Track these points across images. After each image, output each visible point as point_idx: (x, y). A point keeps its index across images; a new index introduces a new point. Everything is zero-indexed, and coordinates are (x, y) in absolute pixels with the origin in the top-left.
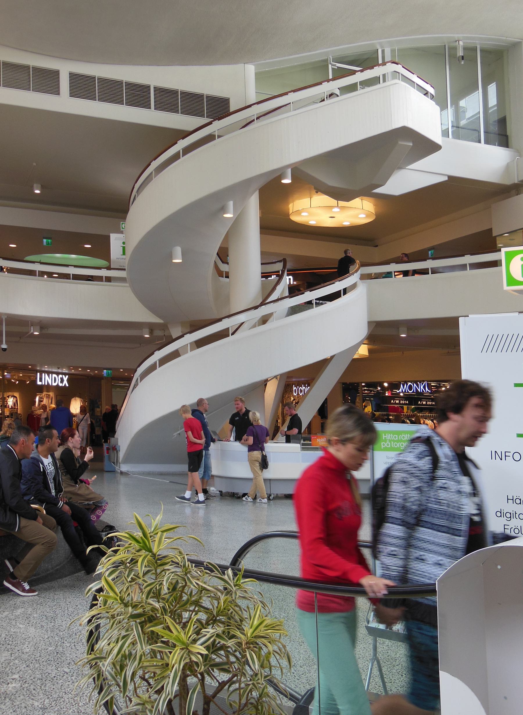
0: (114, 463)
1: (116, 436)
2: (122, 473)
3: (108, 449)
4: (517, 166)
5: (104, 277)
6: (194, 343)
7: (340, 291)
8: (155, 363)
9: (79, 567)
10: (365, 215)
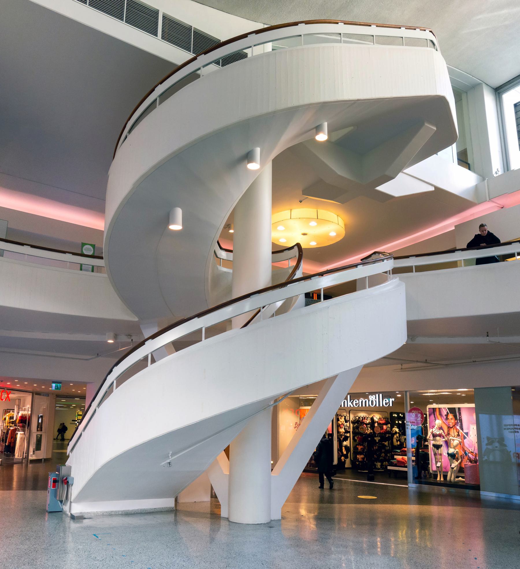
0: (61, 502)
2: (73, 517)
3: (55, 481)
6: (172, 344)
8: (200, 331)
9: (81, 520)
10: (316, 243)
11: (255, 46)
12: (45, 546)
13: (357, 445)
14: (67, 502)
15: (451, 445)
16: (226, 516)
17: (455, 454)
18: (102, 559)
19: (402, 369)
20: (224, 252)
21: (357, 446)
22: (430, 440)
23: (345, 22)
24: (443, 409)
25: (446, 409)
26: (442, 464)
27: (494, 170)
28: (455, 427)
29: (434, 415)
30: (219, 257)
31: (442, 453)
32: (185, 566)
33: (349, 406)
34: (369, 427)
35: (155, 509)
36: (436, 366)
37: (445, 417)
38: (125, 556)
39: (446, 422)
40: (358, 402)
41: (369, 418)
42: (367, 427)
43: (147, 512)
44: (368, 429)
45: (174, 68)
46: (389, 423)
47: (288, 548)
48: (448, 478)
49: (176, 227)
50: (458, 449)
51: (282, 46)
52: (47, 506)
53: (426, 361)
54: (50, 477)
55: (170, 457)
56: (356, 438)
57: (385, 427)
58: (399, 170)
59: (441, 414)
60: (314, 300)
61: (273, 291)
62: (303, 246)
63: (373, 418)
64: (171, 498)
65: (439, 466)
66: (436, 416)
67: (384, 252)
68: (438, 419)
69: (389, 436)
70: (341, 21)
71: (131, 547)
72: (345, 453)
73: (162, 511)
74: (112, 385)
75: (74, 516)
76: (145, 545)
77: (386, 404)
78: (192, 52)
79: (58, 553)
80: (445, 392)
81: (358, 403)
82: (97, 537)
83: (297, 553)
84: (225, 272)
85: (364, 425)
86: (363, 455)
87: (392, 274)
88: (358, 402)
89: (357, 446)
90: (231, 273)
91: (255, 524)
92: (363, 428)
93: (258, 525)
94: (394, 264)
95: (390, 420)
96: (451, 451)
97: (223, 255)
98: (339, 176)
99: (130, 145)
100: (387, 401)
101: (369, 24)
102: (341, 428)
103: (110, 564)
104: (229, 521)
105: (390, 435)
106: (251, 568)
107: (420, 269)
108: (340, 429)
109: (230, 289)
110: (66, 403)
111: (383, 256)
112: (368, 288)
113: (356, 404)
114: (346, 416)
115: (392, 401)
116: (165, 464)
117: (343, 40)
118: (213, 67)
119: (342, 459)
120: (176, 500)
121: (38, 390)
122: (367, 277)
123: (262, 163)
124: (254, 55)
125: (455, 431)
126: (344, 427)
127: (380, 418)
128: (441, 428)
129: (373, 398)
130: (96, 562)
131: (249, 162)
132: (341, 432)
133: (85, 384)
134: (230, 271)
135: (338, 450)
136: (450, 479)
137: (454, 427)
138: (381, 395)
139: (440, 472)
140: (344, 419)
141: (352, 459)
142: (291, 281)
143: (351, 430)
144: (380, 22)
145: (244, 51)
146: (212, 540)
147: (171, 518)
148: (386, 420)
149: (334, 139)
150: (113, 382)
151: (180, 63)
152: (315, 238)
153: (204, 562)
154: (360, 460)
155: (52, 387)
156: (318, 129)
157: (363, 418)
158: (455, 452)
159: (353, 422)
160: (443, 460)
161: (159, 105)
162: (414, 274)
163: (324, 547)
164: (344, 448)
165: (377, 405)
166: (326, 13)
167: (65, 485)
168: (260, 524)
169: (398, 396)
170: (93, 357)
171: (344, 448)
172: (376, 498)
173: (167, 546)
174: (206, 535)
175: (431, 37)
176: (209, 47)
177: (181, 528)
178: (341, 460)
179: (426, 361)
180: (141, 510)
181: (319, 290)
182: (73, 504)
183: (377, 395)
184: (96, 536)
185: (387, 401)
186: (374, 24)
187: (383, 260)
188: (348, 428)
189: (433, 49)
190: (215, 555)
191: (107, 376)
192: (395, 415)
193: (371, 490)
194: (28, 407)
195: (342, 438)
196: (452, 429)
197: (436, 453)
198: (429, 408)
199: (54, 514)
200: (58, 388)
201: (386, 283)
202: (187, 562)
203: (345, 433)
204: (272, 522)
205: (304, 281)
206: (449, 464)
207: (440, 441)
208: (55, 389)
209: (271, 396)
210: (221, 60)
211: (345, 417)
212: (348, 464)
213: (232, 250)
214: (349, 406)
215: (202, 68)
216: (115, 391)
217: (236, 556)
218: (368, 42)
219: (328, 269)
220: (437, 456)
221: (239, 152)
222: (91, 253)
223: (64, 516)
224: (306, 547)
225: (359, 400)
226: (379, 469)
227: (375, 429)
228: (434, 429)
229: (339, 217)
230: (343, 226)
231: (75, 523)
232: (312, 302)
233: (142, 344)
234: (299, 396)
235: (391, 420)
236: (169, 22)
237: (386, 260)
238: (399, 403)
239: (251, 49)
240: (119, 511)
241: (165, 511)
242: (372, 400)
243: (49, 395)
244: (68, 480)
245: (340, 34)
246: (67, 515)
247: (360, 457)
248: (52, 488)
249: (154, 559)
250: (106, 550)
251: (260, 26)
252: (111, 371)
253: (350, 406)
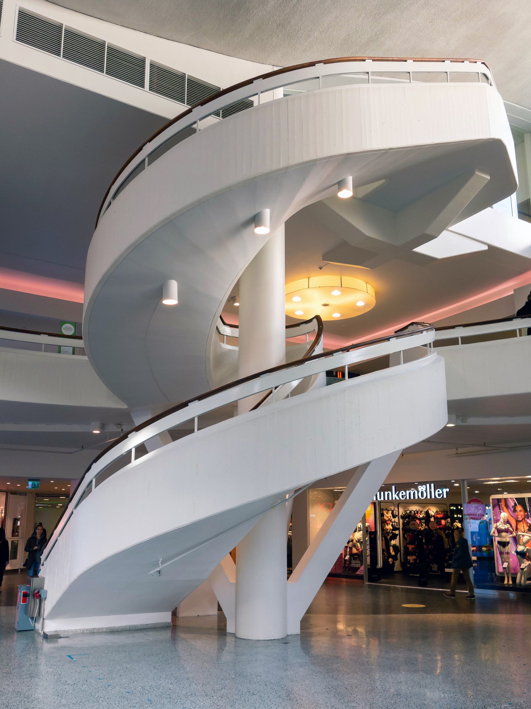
1: (40, 574)
2: (46, 637)
3: (25, 595)
9: (56, 640)
11: (262, 92)
12: (8, 669)
13: (407, 544)
14: (40, 620)
15: (521, 541)
16: (233, 632)
17: (526, 553)
18: (74, 683)
19: (457, 453)
20: (228, 328)
21: (408, 546)
22: (495, 537)
23: (374, 58)
24: (510, 500)
25: (514, 500)
26: (511, 565)
28: (525, 520)
29: (499, 507)
30: (222, 333)
31: (510, 551)
32: (171, 689)
33: (394, 499)
34: (423, 522)
35: (147, 625)
36: (497, 449)
37: (512, 509)
38: (101, 679)
39: (514, 515)
40: (404, 494)
41: (423, 512)
42: (420, 522)
43: (137, 629)
44: (422, 525)
45: (167, 123)
46: (448, 517)
47: (301, 667)
48: (518, 581)
49: (171, 301)
50: (529, 547)
51: (295, 90)
52: (16, 623)
53: (485, 444)
54: (19, 591)
55: (160, 565)
56: (406, 536)
57: (443, 522)
58: (443, 227)
59: (507, 506)
60: (338, 379)
61: (288, 370)
62: (323, 319)
63: (428, 512)
64: (167, 612)
65: (506, 567)
66: (501, 508)
67: (424, 323)
68: (504, 511)
69: (449, 532)
70: (369, 57)
71: (110, 669)
72: (393, 553)
73: (155, 628)
74: (91, 485)
75: (48, 635)
76: (128, 666)
77: (439, 495)
78: (186, 103)
79: (22, 677)
80: (511, 480)
81: (404, 495)
82: (72, 659)
83: (311, 672)
84: (230, 350)
85: (417, 521)
86: (416, 556)
87: (433, 347)
88: (404, 494)
89: (408, 546)
90: (237, 351)
91: (267, 640)
92: (414, 524)
93: (270, 642)
94: (436, 335)
95: (450, 513)
96: (520, 548)
97: (227, 331)
98: (368, 237)
99: (115, 212)
100: (441, 492)
101: (404, 59)
102: (388, 524)
103: (82, 688)
104: (236, 637)
105: (450, 531)
106: (251, 689)
107: (467, 340)
108: (387, 526)
109: (236, 369)
110: (50, 502)
111: (422, 327)
112: (403, 363)
113: (403, 496)
114: (394, 510)
115: (447, 491)
116: (154, 573)
117: (372, 79)
118: (213, 120)
119: (389, 561)
120: (174, 614)
121: (13, 489)
122: (402, 352)
123: (273, 227)
124: (260, 104)
126: (391, 523)
127: (437, 512)
128: (508, 522)
129: (423, 489)
130: (66, 687)
131: (256, 227)
132: (388, 529)
133: (69, 481)
134: (236, 348)
135: (383, 551)
136: (520, 582)
137: (523, 521)
138: (432, 485)
139: (508, 574)
140: (391, 513)
141: (403, 561)
142: (309, 358)
143: (401, 527)
144: (418, 56)
145: (249, 99)
146: (218, 659)
147: (167, 635)
148: (444, 514)
149: (360, 196)
150: (91, 481)
151: (172, 117)
152: (338, 308)
153: (196, 684)
154: (411, 562)
155: (28, 485)
156: (341, 184)
157: (416, 512)
158: (525, 550)
159: (403, 517)
160: (511, 560)
161: (148, 166)
162: (460, 346)
163: (345, 665)
164: (391, 548)
165: (429, 497)
166: (351, 49)
167: (37, 599)
168: (273, 640)
169: (455, 485)
170: (78, 449)
171: (391, 548)
172: (425, 606)
173: (154, 667)
174: (205, 654)
175: (483, 69)
176: (213, 94)
177: (181, 646)
178: (388, 562)
179: (485, 444)
180: (130, 626)
181: (343, 368)
182: (46, 622)
183: (428, 485)
184: (71, 657)
185: (441, 492)
186: (410, 59)
187: (421, 332)
188: (397, 524)
189: (487, 84)
190: (211, 676)
191: (85, 474)
192: (453, 508)
193: (421, 597)
194: (2, 509)
195: (389, 537)
196: (522, 523)
197: (503, 551)
198: (492, 499)
199: (24, 633)
200: (35, 487)
201: (426, 357)
202: (175, 685)
203: (393, 530)
204: (289, 638)
205: (325, 358)
206: (519, 564)
207: (507, 537)
208: (32, 487)
209: (276, 493)
210: (221, 111)
211: (393, 511)
212: (397, 567)
213: (238, 325)
214: (394, 499)
215: (198, 122)
216: (95, 490)
217: (235, 676)
218: (404, 79)
219: (354, 344)
220: (503, 555)
221: (244, 215)
222: (71, 333)
223: (36, 635)
224: (324, 665)
225: (405, 492)
226: (435, 572)
227: (430, 525)
228: (498, 524)
229: (367, 284)
230: (374, 295)
231: (47, 644)
232: (335, 381)
234: (333, 488)
235: (448, 514)
236: (157, 71)
237: (426, 331)
238: (454, 493)
239: (257, 96)
240: (103, 629)
241: (159, 627)
242: (422, 490)
243: (27, 494)
244: (40, 593)
245: (368, 73)
246: (39, 634)
247: (411, 558)
248: (22, 603)
249: (136, 682)
250: (80, 673)
251: (269, 69)
252: (89, 468)
253: (395, 498)
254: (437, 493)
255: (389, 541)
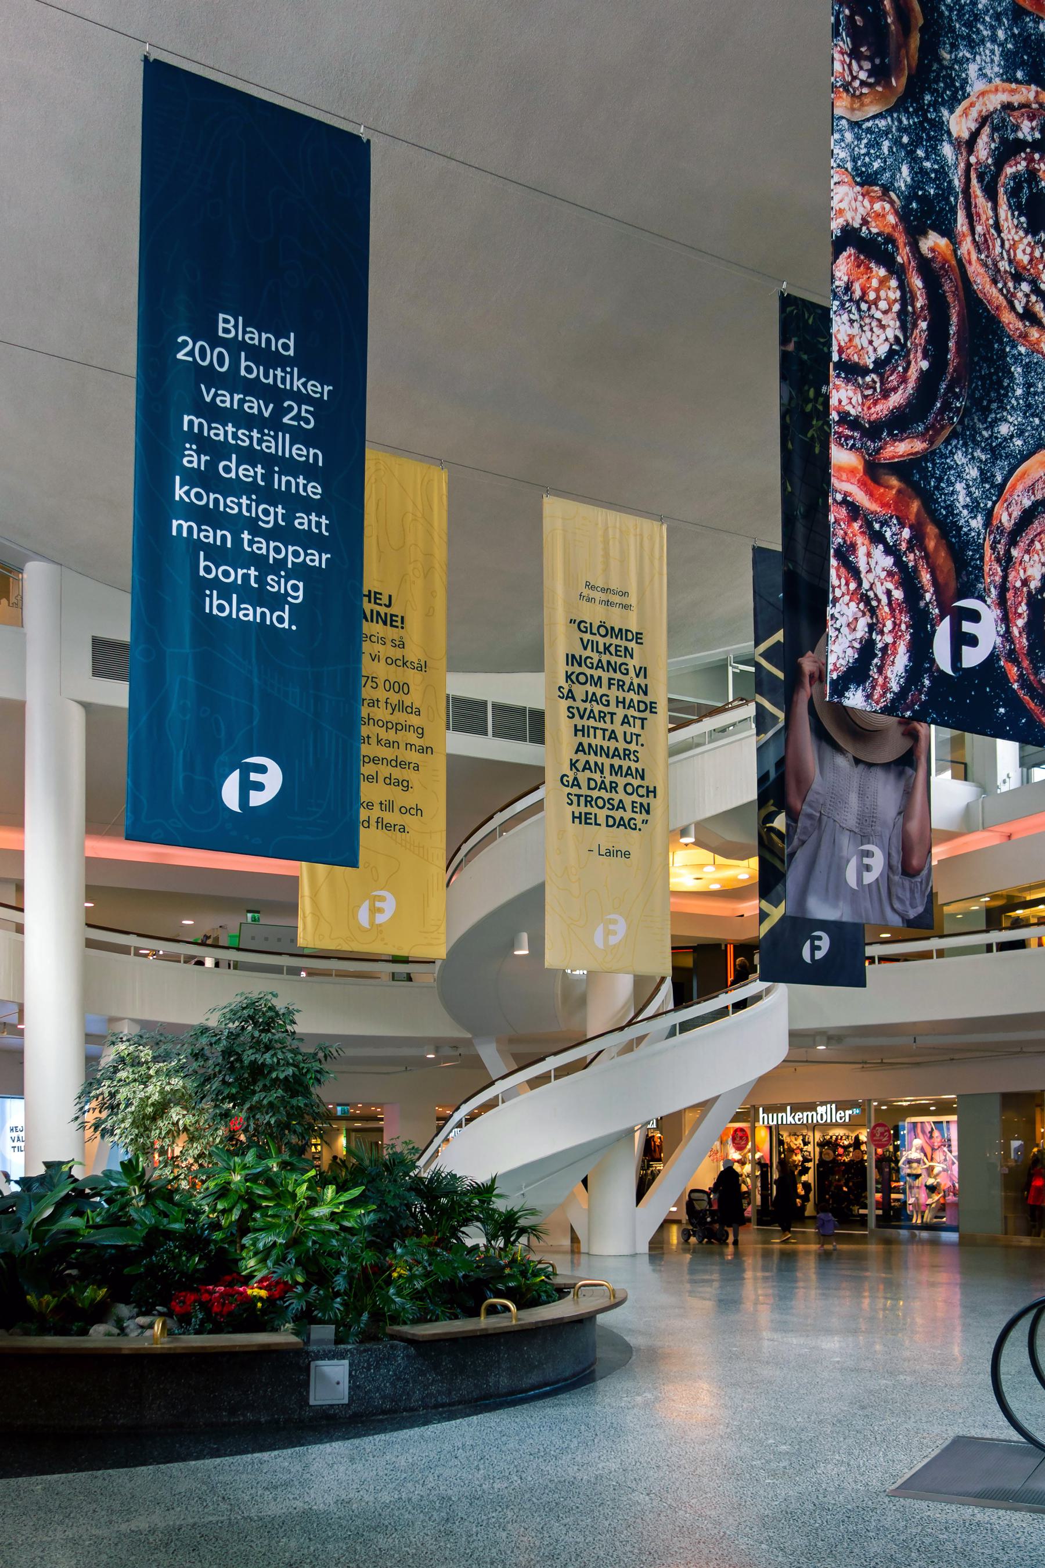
4: (983, 808)
5: (285, 968)
7: (727, 1007)
27: (1001, 775)
77: (841, 1118)
125: (941, 1154)
138: (834, 1106)
139: (917, 1212)
159: (821, 1145)
207: (917, 1169)
233: (492, 1083)
254: (838, 1115)
255: (797, 1177)
